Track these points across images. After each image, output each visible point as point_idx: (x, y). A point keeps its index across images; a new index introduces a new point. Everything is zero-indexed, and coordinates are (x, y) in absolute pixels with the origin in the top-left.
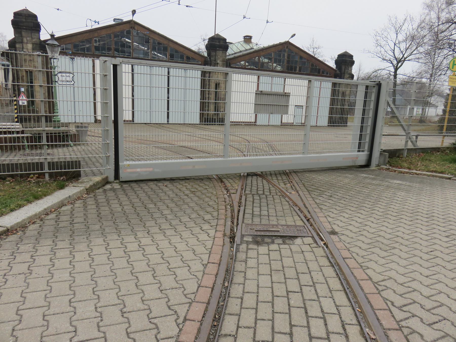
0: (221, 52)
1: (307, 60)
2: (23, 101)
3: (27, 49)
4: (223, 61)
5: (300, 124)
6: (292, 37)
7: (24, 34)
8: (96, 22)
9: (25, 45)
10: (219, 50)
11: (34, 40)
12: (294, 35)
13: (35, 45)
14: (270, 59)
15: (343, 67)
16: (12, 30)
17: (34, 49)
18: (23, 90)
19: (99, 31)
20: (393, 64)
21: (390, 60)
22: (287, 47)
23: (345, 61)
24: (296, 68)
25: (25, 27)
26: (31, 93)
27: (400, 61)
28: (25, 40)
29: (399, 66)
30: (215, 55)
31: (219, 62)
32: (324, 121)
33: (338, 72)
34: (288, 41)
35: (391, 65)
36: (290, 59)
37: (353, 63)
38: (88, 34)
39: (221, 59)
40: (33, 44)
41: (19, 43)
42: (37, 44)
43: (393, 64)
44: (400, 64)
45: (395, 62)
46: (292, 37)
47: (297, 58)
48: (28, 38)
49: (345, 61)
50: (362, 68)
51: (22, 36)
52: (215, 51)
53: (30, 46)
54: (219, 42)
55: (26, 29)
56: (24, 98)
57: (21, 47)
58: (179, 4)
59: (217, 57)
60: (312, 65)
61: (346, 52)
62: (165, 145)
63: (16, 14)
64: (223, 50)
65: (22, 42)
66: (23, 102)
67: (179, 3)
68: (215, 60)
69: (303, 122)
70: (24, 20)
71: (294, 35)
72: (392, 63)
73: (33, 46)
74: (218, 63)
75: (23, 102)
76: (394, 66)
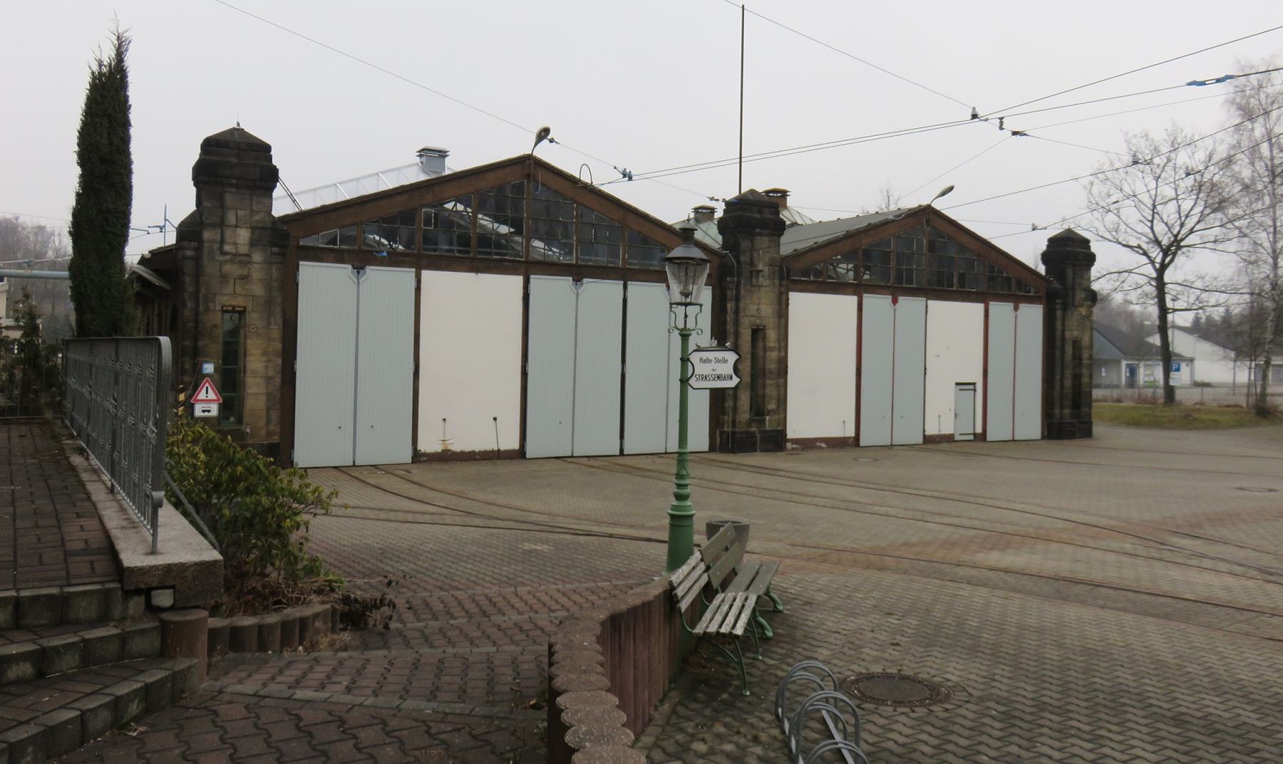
0: (766, 239)
1: (979, 256)
2: (207, 403)
3: (236, 244)
4: (771, 264)
5: (972, 437)
6: (944, 193)
7: (229, 199)
8: (625, 176)
9: (228, 233)
10: (761, 235)
11: (256, 218)
12: (951, 189)
13: (257, 232)
14: (517, 225)
15: (1070, 273)
16: (193, 191)
17: (253, 243)
18: (209, 368)
19: (437, 188)
20: (1149, 257)
21: (1139, 247)
22: (928, 221)
23: (1069, 253)
24: (951, 277)
25: (234, 181)
26: (230, 384)
27: (1172, 249)
28: (231, 218)
29: (1167, 260)
30: (752, 250)
31: (760, 267)
32: (1031, 426)
33: (1056, 285)
34: (929, 206)
35: (1144, 260)
36: (918, 255)
37: (1091, 259)
38: (405, 196)
39: (766, 259)
40: (253, 229)
41: (213, 226)
42: (263, 228)
43: (1149, 257)
44: (1167, 260)
45: (1157, 254)
46: (944, 193)
47: (952, 252)
48: (241, 213)
49: (1069, 253)
50: (1117, 274)
51: (223, 207)
52: (751, 236)
53: (244, 235)
54: (760, 212)
55: (237, 186)
56: (212, 395)
57: (218, 238)
58: (1001, 128)
59: (755, 254)
60: (992, 269)
61: (1069, 230)
62: (973, 572)
63: (210, 145)
64: (773, 235)
65: (222, 224)
66: (206, 406)
67: (1001, 123)
68: (752, 264)
69: (979, 430)
70: (234, 160)
71: (951, 189)
72: (1145, 254)
73: (253, 233)
74: (759, 272)
75: (206, 406)
76: (1152, 262)
